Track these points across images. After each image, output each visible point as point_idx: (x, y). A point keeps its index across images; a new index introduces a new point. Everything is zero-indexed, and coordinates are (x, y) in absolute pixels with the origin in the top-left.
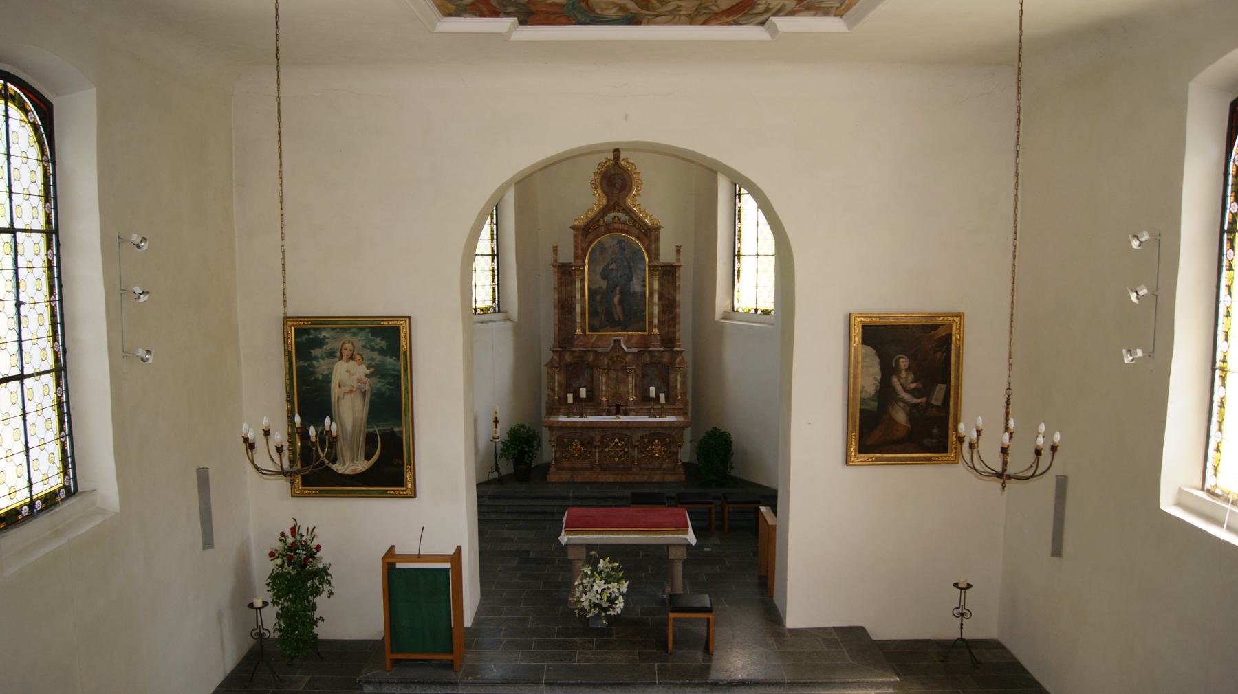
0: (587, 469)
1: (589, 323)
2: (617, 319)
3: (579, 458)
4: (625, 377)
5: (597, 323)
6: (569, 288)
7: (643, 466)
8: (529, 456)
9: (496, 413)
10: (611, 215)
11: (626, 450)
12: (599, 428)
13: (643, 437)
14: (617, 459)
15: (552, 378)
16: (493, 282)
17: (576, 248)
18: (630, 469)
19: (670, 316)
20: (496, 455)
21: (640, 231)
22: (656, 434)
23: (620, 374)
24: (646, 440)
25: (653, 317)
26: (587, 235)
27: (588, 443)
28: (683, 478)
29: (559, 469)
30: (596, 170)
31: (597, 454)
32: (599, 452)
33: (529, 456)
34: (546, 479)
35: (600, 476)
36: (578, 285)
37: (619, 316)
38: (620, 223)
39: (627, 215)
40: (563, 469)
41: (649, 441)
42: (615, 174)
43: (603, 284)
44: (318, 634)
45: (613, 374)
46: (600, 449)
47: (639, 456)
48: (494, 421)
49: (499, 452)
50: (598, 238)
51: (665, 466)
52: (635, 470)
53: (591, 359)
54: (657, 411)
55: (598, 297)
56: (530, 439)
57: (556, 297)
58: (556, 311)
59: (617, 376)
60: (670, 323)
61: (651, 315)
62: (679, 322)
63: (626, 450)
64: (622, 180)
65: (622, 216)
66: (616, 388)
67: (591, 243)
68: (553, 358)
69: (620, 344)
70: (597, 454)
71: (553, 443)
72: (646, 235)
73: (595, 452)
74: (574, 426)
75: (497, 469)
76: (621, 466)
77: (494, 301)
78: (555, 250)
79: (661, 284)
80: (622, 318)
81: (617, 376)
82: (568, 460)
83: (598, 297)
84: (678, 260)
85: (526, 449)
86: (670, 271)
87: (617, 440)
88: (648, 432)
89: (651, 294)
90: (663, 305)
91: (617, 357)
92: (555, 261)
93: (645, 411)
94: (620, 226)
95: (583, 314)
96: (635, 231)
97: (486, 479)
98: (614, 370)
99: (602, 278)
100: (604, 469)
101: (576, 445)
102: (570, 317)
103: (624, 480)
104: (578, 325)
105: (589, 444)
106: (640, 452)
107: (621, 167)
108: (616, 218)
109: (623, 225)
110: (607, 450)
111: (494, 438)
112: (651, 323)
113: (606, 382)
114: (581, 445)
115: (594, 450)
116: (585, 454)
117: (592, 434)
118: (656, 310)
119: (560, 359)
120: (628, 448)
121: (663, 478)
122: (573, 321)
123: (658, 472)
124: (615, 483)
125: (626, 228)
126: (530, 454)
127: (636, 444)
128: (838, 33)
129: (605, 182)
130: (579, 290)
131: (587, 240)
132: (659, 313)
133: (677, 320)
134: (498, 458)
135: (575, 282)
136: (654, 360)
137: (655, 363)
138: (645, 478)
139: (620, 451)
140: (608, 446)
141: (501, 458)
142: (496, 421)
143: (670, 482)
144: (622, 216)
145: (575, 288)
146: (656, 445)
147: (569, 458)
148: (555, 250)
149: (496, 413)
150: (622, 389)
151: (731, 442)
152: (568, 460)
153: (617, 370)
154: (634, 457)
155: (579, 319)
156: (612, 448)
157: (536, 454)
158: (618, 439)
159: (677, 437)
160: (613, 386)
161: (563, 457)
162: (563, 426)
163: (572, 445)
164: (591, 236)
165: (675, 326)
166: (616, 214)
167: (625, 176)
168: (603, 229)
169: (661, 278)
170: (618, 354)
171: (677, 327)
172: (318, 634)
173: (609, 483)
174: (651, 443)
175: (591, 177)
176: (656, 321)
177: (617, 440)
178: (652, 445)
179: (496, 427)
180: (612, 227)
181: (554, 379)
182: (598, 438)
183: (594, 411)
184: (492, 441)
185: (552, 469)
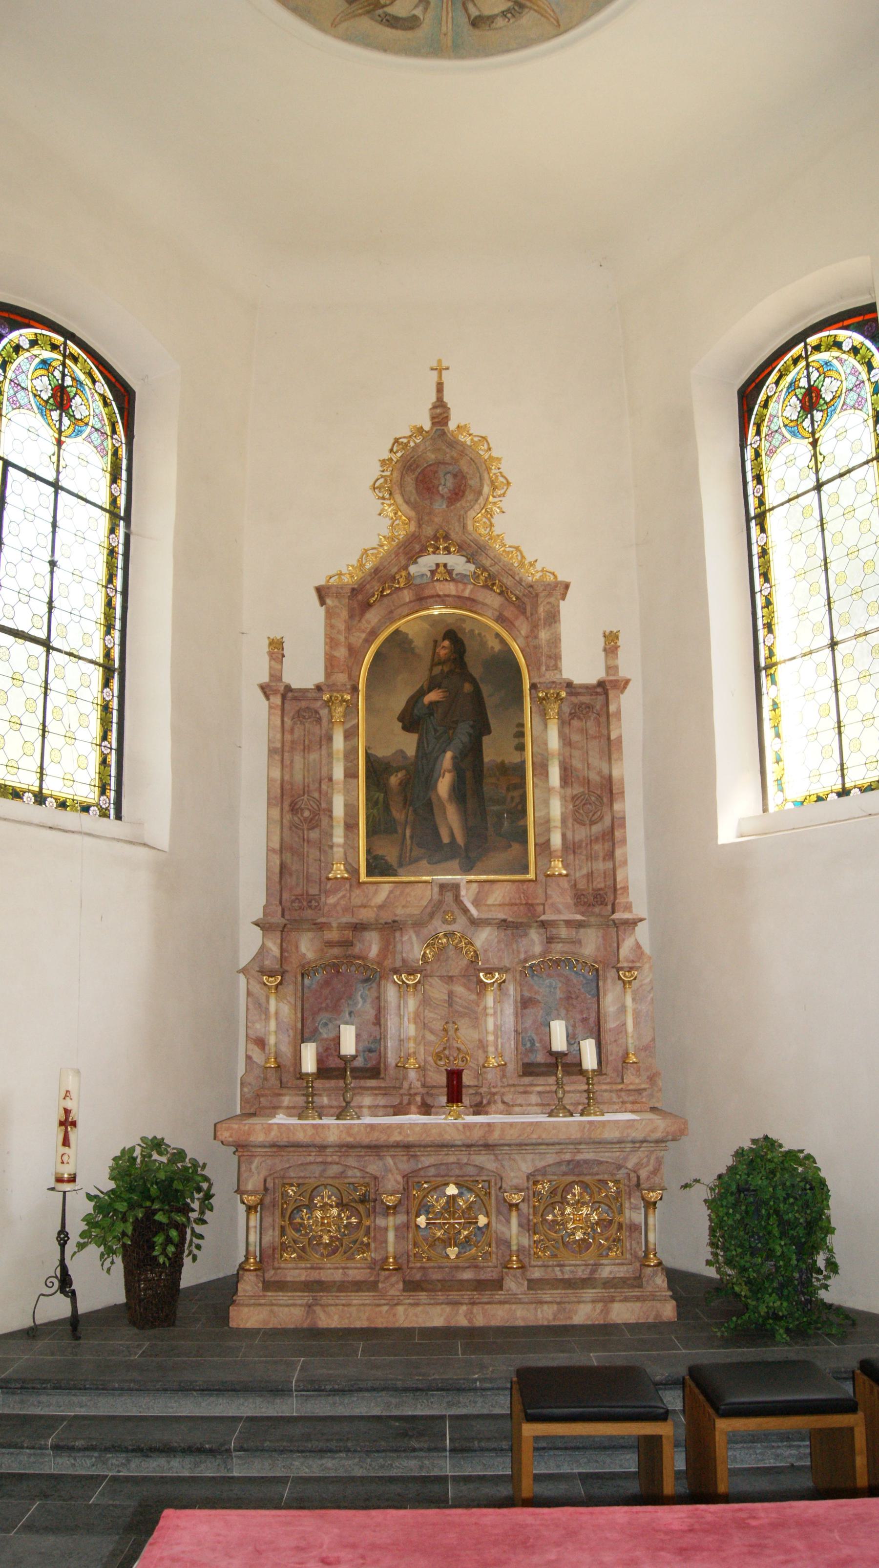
0: (358, 1286)
1: (369, 851)
2: (446, 840)
3: (334, 1252)
4: (474, 997)
5: (390, 854)
6: (313, 756)
7: (537, 1274)
8: (169, 1240)
9: (67, 1095)
10: (427, 562)
11: (482, 1220)
12: (397, 1145)
13: (533, 1178)
14: (452, 1252)
15: (259, 1007)
16: (104, 738)
17: (331, 642)
18: (498, 1284)
19: (596, 829)
20: (63, 1237)
21: (508, 600)
22: (575, 1167)
23: (459, 989)
24: (544, 1188)
25: (548, 830)
26: (363, 612)
27: (363, 1200)
28: (668, 1311)
29: (267, 1286)
30: (386, 455)
31: (391, 1236)
32: (397, 1228)
33: (169, 1240)
34: (226, 1319)
35: (400, 1309)
36: (339, 742)
37: (452, 835)
38: (453, 580)
39: (468, 561)
40: (280, 1286)
41: (553, 1192)
42: (439, 463)
43: (408, 743)
44: (705, 1201)
45: (438, 991)
46: (401, 1219)
47: (525, 1242)
48: (74, 1124)
49: (76, 1227)
50: (393, 621)
51: (605, 1272)
52: (510, 1284)
53: (374, 951)
54: (575, 1097)
55: (394, 780)
56: (177, 1185)
57: (277, 774)
58: (276, 813)
59: (451, 994)
60: (597, 847)
61: (545, 824)
62: (624, 841)
63: (482, 1220)
64: (455, 476)
65: (458, 563)
66: (445, 1030)
67: (373, 634)
68: (263, 946)
69: (457, 898)
70: (391, 1236)
71: (251, 1199)
72: (521, 609)
73: (386, 1229)
74: (318, 1140)
75: (65, 1282)
76: (467, 1275)
77: (103, 790)
78: (277, 648)
79: (566, 741)
80: (460, 839)
81: (451, 994)
82: (300, 1257)
83: (394, 780)
84: (611, 669)
85: (160, 1217)
86: (589, 707)
87: (452, 1190)
88: (551, 1159)
89: (542, 769)
90: (574, 798)
91: (449, 935)
92: (276, 676)
93: (534, 1099)
94: (451, 588)
95: (351, 826)
96: (493, 600)
97: (27, 1323)
98: (441, 977)
99: (405, 728)
100: (412, 1286)
101: (324, 1207)
102: (314, 835)
103: (480, 1321)
104: (338, 852)
105: (382, 1242)
106: (528, 1227)
107: (453, 444)
108: (441, 569)
109: (461, 586)
110: (422, 1221)
111: (59, 1180)
112: (544, 847)
113: (417, 1015)
114: (341, 1205)
115: (381, 1222)
116: (354, 1237)
117: (374, 1167)
118: (556, 809)
119: (282, 950)
120: (487, 1215)
121: (606, 1311)
122: (324, 846)
123: (589, 1293)
124: (449, 1333)
125: (467, 594)
126: (174, 1233)
127: (516, 1198)
128: (355, 1508)
129: (410, 480)
130: (341, 756)
131: (364, 624)
132: (564, 821)
133: (618, 834)
134: (70, 1247)
135: (330, 739)
136: (558, 950)
137: (557, 962)
138: (545, 1315)
139: (464, 1226)
140: (424, 1208)
141: (81, 1246)
142: (67, 1122)
143: (627, 1325)
144: (458, 563)
145: (330, 755)
146: (579, 1203)
147: (303, 1249)
148: (277, 648)
149: (67, 1095)
150: (466, 1035)
151: (822, 1183)
152: (300, 1257)
153: (450, 979)
154: (508, 1244)
155: (338, 836)
156: (440, 1215)
157: (201, 1237)
158: (458, 1185)
159: (643, 1174)
160: (438, 1026)
161: (284, 1247)
162: (284, 1140)
163: (311, 1207)
164: (373, 617)
165: (610, 855)
166: (442, 558)
167: (464, 465)
168: (407, 595)
169: (563, 723)
170: (450, 928)
171: (618, 852)
172: (705, 1201)
173: (428, 1333)
174: (558, 1197)
175: (374, 471)
176: (556, 840)
177: (452, 1190)
178: (564, 1202)
179: (66, 1142)
180: (428, 592)
181: (267, 1009)
182: (393, 1181)
183: (381, 1101)
184: (52, 1189)
185: (248, 1286)
